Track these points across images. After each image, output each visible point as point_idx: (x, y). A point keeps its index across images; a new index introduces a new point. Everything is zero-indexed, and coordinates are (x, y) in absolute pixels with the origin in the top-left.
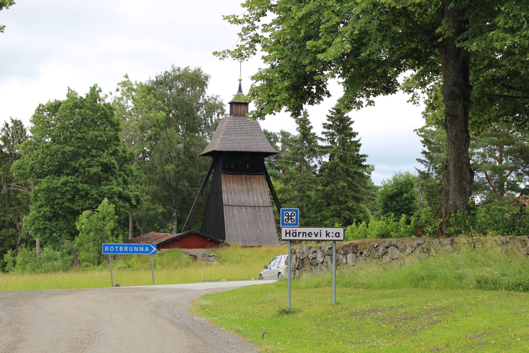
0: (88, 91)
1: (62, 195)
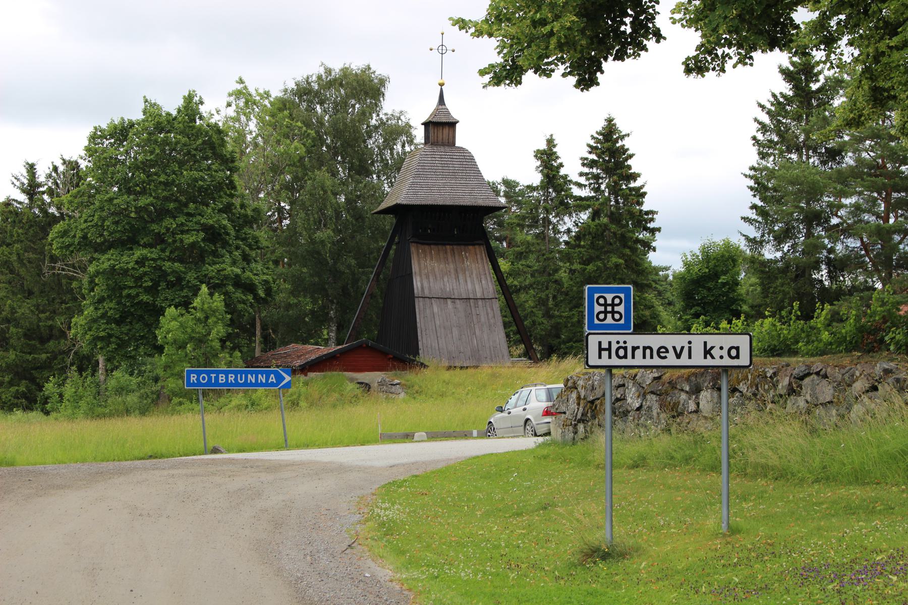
0: (180, 102)
1: (135, 282)
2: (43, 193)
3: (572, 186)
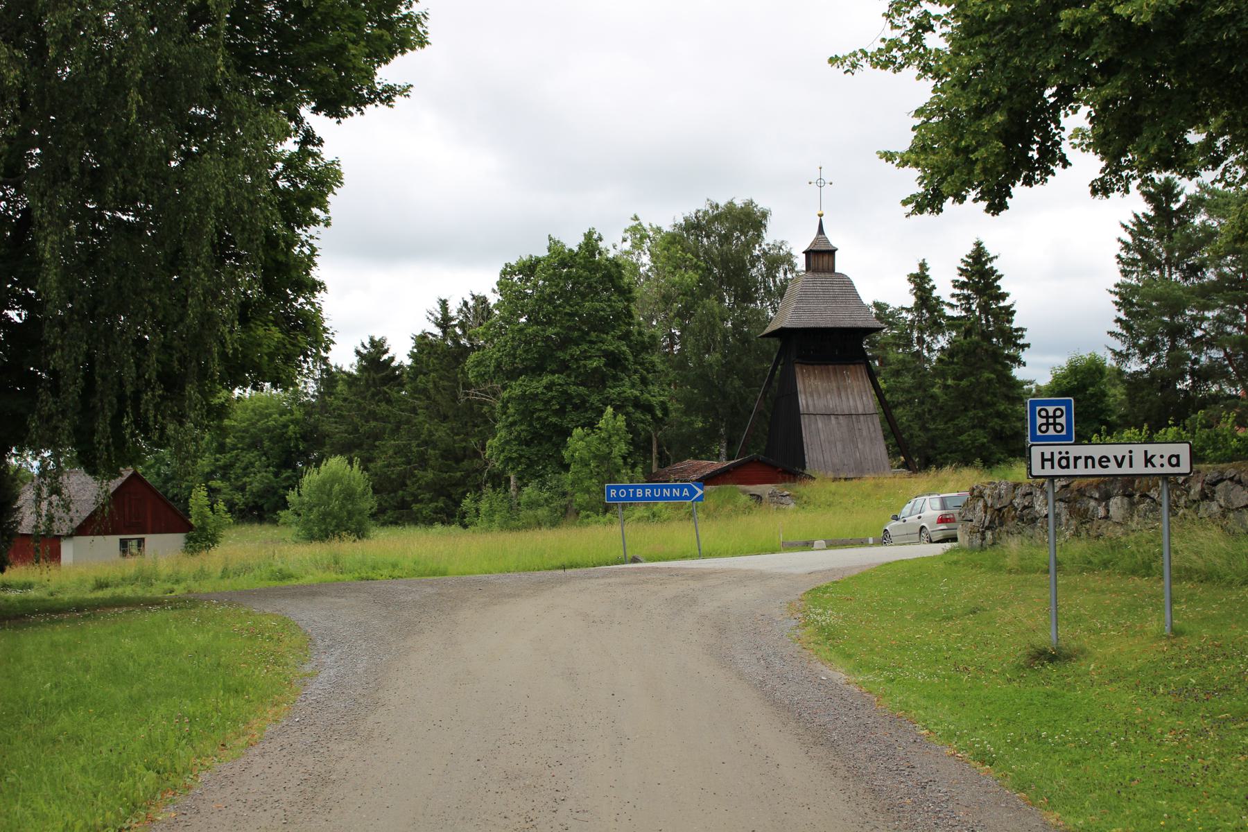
0: (581, 240)
2: (455, 326)
3: (944, 307)
